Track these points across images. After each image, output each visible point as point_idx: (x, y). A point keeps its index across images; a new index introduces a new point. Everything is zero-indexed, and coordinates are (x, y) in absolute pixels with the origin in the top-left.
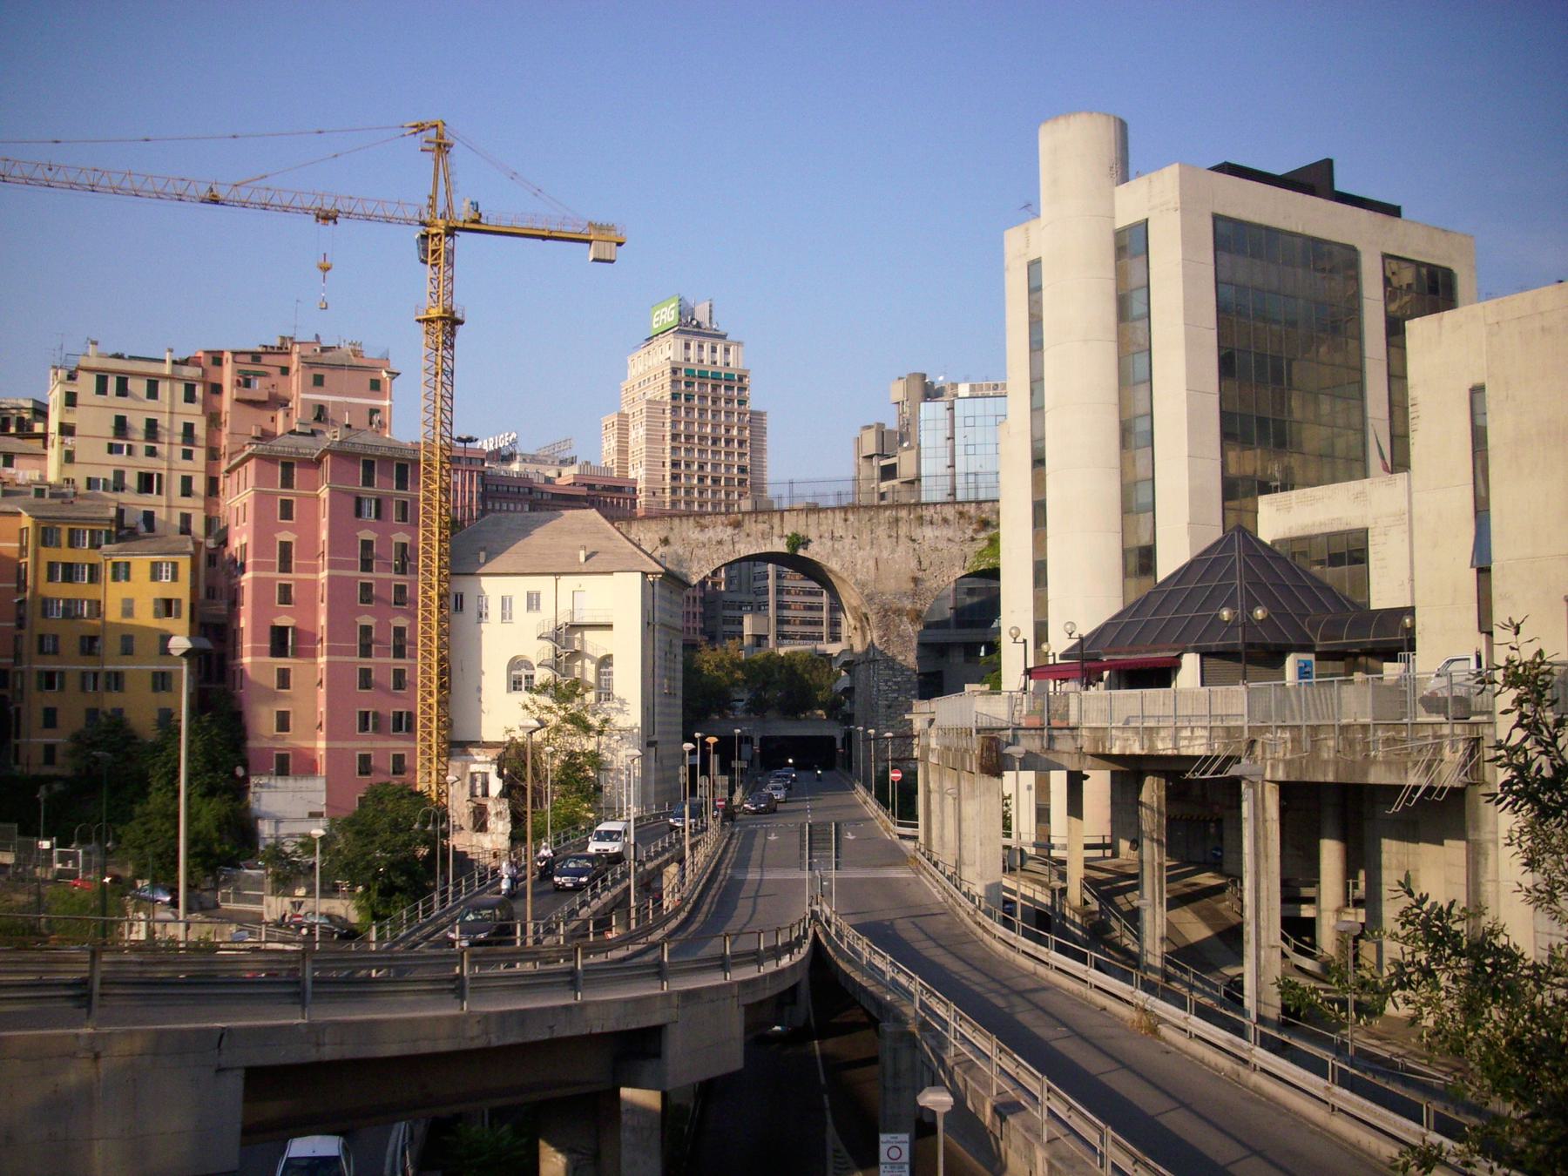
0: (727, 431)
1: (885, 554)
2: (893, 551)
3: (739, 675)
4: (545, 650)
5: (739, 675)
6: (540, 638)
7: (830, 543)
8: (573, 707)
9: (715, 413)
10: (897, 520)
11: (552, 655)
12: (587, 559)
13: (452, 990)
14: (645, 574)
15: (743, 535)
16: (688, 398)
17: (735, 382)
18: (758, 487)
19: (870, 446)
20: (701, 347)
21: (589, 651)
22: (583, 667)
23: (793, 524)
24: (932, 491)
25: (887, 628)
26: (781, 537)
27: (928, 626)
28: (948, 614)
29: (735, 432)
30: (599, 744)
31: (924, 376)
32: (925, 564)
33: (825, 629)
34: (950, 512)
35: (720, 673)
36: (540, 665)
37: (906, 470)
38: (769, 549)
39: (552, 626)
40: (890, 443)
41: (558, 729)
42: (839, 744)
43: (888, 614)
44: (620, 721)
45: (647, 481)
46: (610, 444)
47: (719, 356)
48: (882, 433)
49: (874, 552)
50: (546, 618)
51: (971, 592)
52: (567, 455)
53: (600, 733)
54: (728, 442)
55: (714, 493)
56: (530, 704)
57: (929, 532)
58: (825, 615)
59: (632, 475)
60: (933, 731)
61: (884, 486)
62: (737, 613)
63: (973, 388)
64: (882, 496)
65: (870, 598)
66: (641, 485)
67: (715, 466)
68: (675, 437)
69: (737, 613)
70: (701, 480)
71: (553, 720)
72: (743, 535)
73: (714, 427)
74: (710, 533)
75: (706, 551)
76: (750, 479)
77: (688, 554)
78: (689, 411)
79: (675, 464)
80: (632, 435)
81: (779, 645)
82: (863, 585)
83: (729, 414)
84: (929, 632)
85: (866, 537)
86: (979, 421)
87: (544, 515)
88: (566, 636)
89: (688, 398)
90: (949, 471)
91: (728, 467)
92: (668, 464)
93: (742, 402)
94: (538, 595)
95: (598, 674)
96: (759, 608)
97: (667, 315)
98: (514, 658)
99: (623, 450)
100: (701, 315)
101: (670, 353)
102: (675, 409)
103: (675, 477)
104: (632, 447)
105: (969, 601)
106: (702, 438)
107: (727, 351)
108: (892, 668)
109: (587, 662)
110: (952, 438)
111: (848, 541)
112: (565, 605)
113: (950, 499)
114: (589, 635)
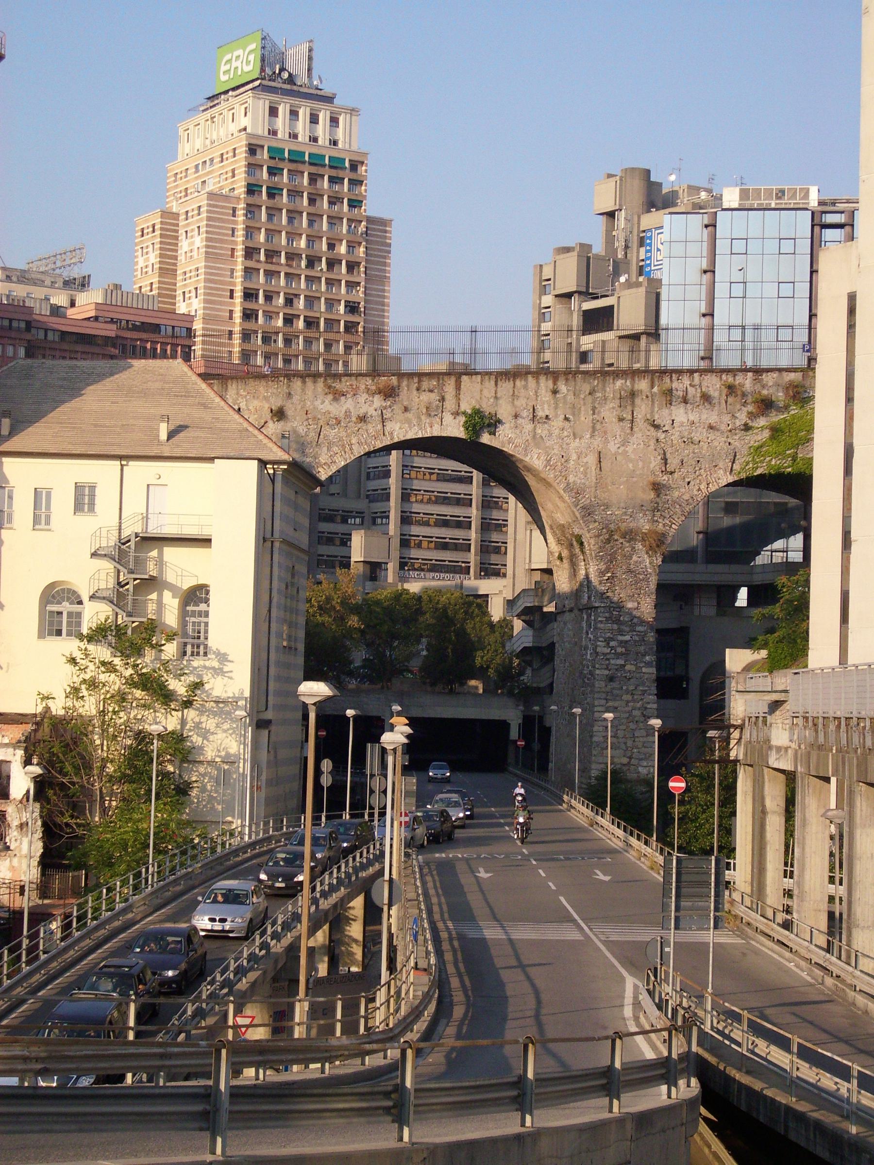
0: (331, 246)
1: (612, 447)
2: (625, 443)
3: (354, 621)
4: (104, 573)
5: (354, 621)
6: (94, 555)
7: (529, 427)
8: (148, 661)
9: (314, 218)
10: (633, 394)
11: (111, 583)
12: (171, 435)
13: (387, 1110)
14: (263, 463)
15: (398, 408)
16: (273, 193)
17: (346, 171)
18: (376, 336)
19: (568, 279)
20: (294, 113)
21: (170, 577)
22: (160, 603)
23: (475, 395)
24: (678, 351)
25: (612, 559)
26: (456, 414)
27: (672, 558)
28: (695, 540)
29: (343, 249)
30: (183, 722)
31: (648, 172)
32: (673, 463)
33: (472, 557)
34: (713, 385)
35: (326, 619)
36: (92, 597)
37: (630, 312)
38: (436, 431)
39: (113, 540)
40: (598, 272)
41: (121, 698)
42: (514, 734)
43: (615, 538)
44: (217, 687)
45: (206, 319)
46: (148, 259)
47: (322, 130)
48: (587, 260)
49: (597, 442)
50: (104, 524)
51: (730, 508)
52: (76, 272)
53: (188, 704)
54: (332, 264)
55: (308, 342)
56: (78, 655)
57: (680, 414)
58: (473, 535)
59: (182, 308)
60: (778, 719)
61: (588, 342)
62: (340, 528)
63: (744, 194)
64: (584, 357)
65: (588, 512)
66: (198, 326)
67: (311, 301)
68: (250, 253)
69: (340, 528)
70: (289, 320)
71: (114, 682)
72: (398, 408)
73: (311, 240)
74: (347, 404)
75: (342, 428)
76: (364, 325)
77: (312, 435)
78: (273, 212)
79: (249, 295)
80: (184, 245)
81: (403, 579)
82: (577, 492)
83: (334, 220)
84: (674, 567)
85: (585, 418)
86: (754, 247)
87: (101, 364)
88: (135, 555)
89: (273, 193)
90: (704, 321)
91: (331, 303)
92: (239, 294)
93: (355, 204)
94: (93, 488)
95: (183, 614)
96: (374, 520)
97: (243, 61)
98: (52, 585)
99: (168, 269)
100: (296, 64)
101: (245, 122)
102: (251, 210)
103: (249, 315)
104: (183, 265)
105: (727, 521)
106: (292, 256)
107: (334, 121)
108: (617, 621)
109: (167, 595)
110: (710, 271)
111: (558, 423)
112: (134, 505)
113: (703, 364)
114: (171, 553)
